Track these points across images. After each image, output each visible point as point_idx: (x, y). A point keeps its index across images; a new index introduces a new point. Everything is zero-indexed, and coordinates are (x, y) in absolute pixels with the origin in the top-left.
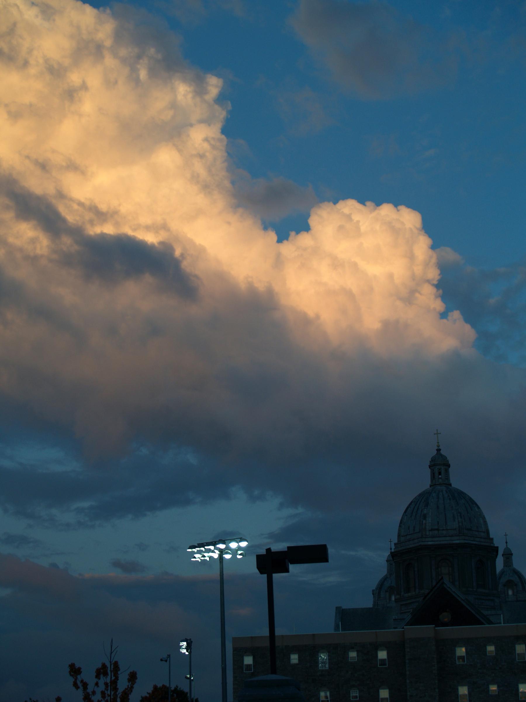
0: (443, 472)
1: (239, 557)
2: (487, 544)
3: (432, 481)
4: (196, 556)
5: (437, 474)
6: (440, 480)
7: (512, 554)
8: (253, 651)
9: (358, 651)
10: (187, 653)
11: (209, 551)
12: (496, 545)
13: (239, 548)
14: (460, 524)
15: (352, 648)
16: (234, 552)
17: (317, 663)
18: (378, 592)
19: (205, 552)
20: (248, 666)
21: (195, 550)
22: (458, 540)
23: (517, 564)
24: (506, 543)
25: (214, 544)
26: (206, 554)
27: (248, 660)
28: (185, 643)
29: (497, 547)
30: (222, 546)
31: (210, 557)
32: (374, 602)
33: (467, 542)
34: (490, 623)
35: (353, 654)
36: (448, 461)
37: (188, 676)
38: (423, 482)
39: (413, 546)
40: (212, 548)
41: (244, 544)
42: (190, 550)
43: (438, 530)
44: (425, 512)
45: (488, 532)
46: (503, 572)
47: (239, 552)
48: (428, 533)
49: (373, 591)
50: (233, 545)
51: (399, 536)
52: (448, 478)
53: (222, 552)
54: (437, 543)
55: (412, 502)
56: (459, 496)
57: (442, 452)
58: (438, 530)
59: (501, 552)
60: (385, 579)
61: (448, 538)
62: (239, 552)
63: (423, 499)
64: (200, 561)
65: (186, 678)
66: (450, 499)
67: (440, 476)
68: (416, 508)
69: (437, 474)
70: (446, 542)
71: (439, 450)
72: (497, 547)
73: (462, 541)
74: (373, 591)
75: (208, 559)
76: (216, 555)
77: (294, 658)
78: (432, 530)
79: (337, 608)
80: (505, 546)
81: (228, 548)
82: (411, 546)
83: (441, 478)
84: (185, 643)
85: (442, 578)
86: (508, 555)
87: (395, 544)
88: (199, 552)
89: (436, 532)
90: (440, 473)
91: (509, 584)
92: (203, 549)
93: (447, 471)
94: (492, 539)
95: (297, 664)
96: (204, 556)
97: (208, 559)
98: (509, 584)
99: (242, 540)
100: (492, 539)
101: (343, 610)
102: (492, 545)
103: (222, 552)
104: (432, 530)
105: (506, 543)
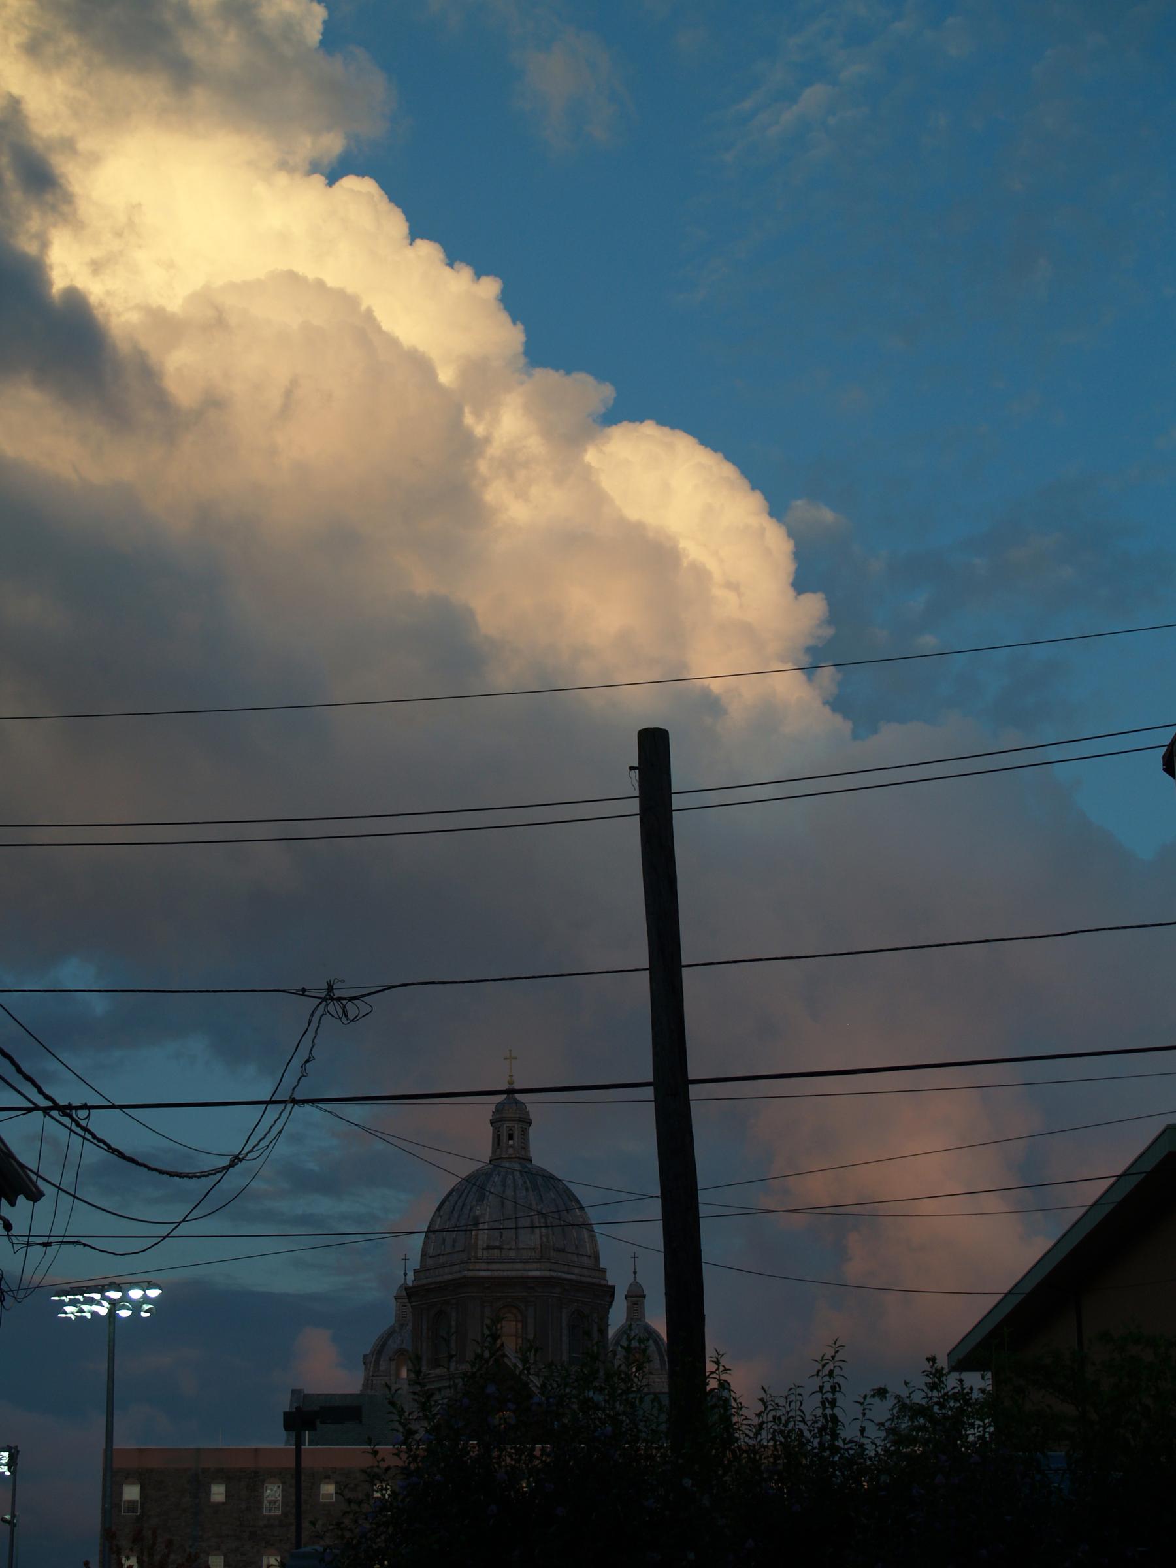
0: (516, 1134)
1: (144, 1315)
2: (594, 1280)
3: (494, 1152)
4: (68, 1309)
5: (504, 1138)
6: (511, 1151)
7: (645, 1296)
8: (143, 1477)
9: (336, 1483)
10: (8, 1473)
11: (91, 1301)
12: (610, 1283)
13: (146, 1299)
14: (544, 1240)
15: (327, 1477)
16: (136, 1306)
17: (259, 1501)
18: (374, 1359)
19: (84, 1303)
20: (132, 1503)
21: (66, 1299)
22: (540, 1270)
24: (635, 1273)
25: (101, 1290)
26: (85, 1308)
27: (132, 1493)
28: (6, 1454)
29: (613, 1288)
30: (115, 1295)
31: (94, 1313)
32: (366, 1380)
33: (554, 1274)
35: (328, 1489)
36: (528, 1114)
37: (8, 1517)
39: (450, 1277)
40: (97, 1296)
41: (154, 1293)
42: (56, 1298)
43: (500, 1248)
44: (477, 1212)
45: (596, 1257)
47: (146, 1307)
48: (480, 1254)
49: (365, 1356)
50: (136, 1294)
51: (424, 1254)
52: (525, 1147)
53: (114, 1304)
54: (496, 1274)
55: (453, 1190)
56: (545, 1181)
58: (500, 1248)
60: (391, 1333)
61: (519, 1266)
62: (146, 1307)
63: (474, 1186)
64: (73, 1318)
65: (4, 1520)
66: (527, 1189)
67: (511, 1142)
68: (456, 1215)
69: (504, 1138)
70: (514, 1274)
72: (613, 1288)
73: (548, 1274)
74: (365, 1356)
75: (88, 1316)
76: (103, 1310)
77: (218, 1493)
78: (489, 1248)
79: (293, 1392)
80: (632, 1280)
81: (126, 1297)
82: (446, 1278)
83: (511, 1146)
84: (6, 1454)
85: (502, 1345)
87: (415, 1272)
88: (73, 1303)
89: (496, 1252)
90: (511, 1137)
92: (80, 1297)
93: (524, 1133)
94: (604, 1271)
95: (223, 1504)
96: (82, 1311)
97: (88, 1316)
99: (151, 1285)
100: (604, 1271)
101: (306, 1396)
102: (603, 1282)
103: (114, 1304)
104: (489, 1248)
105: (635, 1273)
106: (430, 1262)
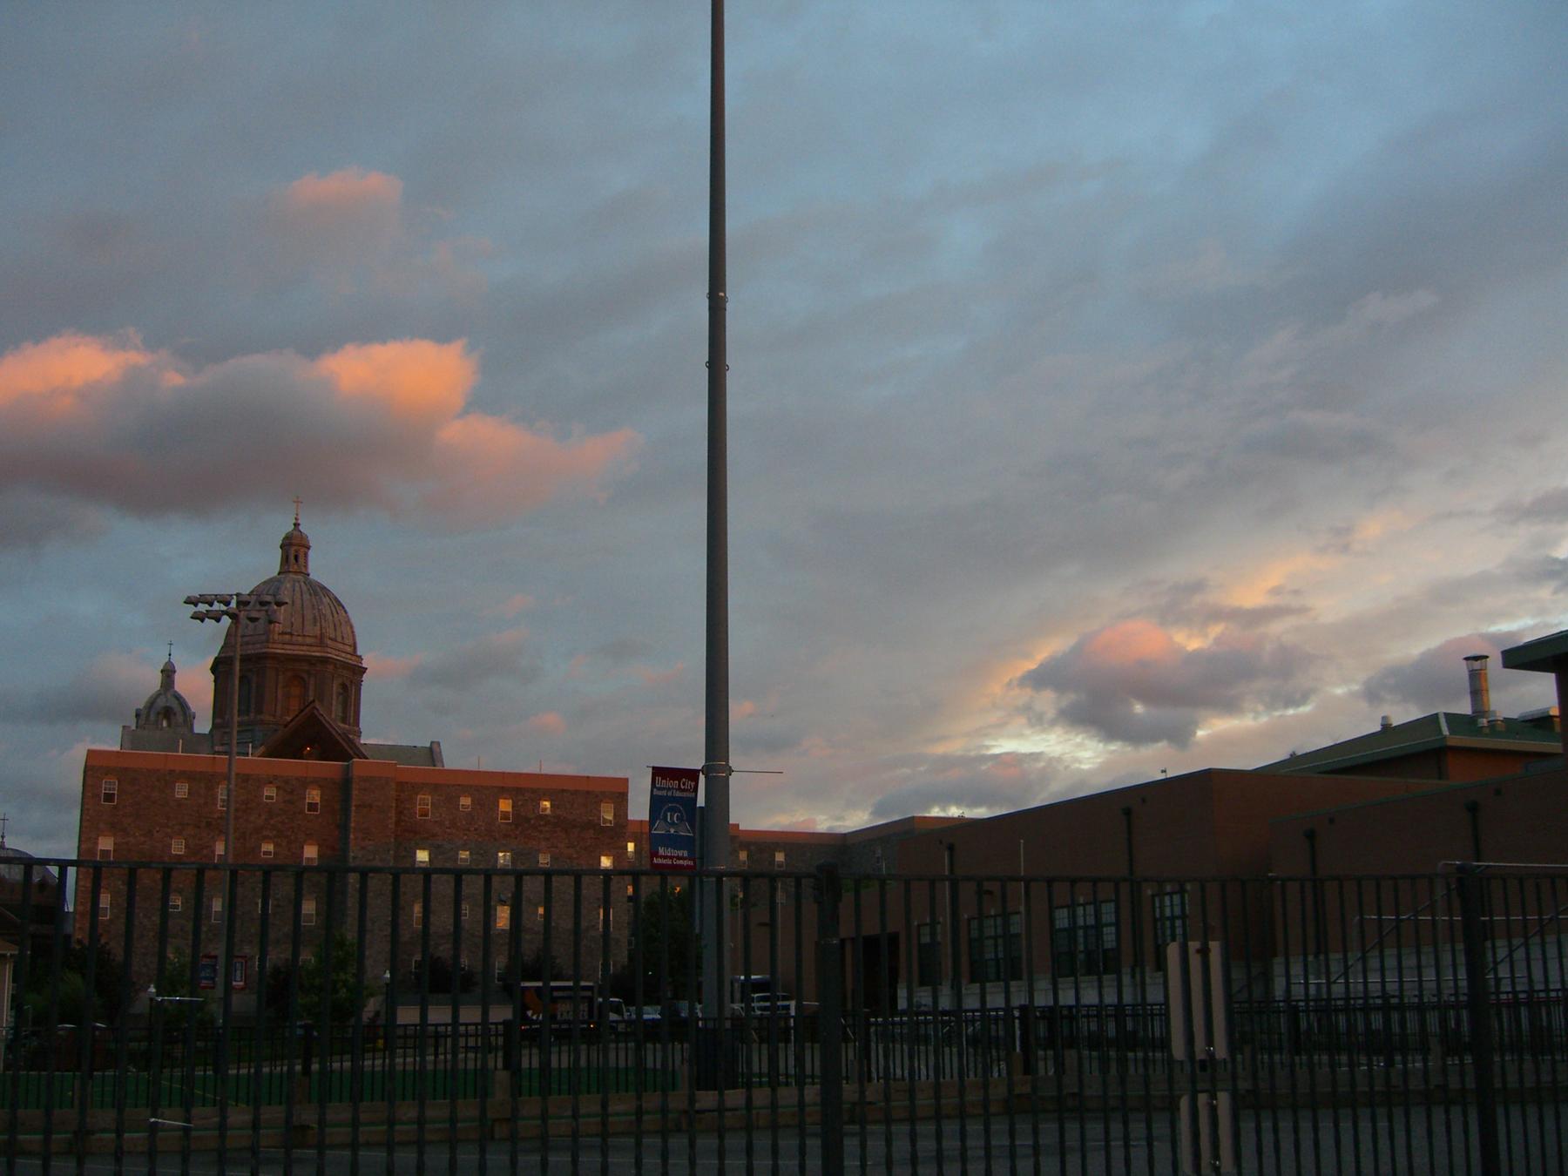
57: (319, 567)
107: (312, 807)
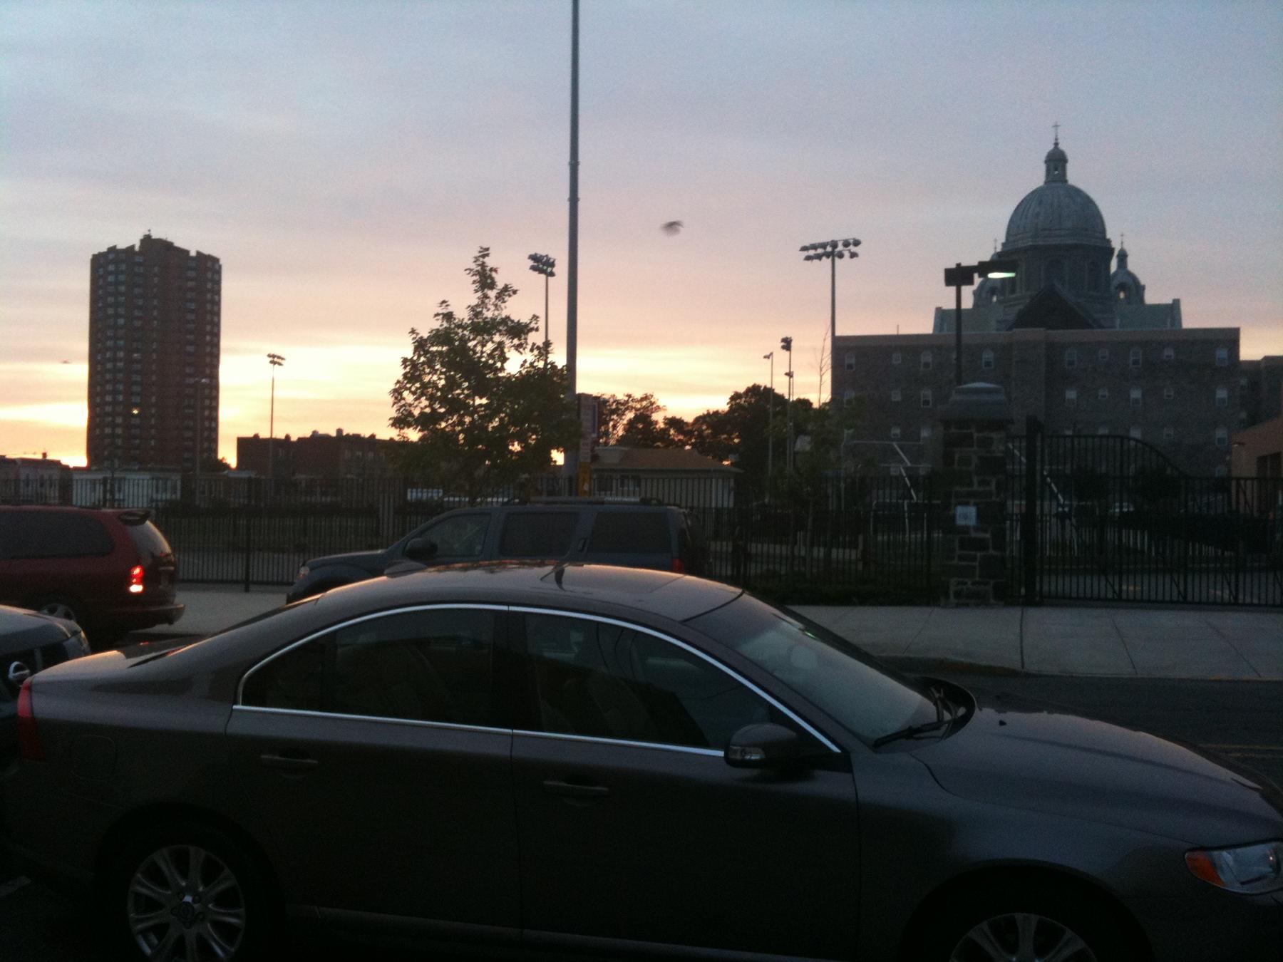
23: (1132, 266)
34: (1101, 327)
38: (1036, 178)
46: (1116, 273)
57: (1075, 176)
59: (1116, 253)
71: (1056, 144)
86: (1123, 257)
91: (1122, 287)
98: (1122, 287)
106: (1011, 239)
107: (988, 364)
